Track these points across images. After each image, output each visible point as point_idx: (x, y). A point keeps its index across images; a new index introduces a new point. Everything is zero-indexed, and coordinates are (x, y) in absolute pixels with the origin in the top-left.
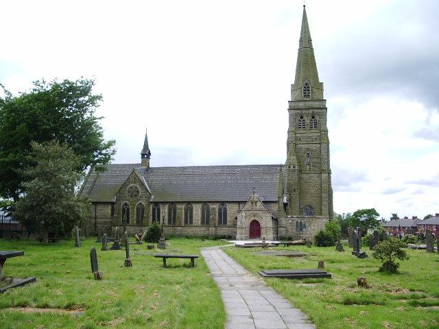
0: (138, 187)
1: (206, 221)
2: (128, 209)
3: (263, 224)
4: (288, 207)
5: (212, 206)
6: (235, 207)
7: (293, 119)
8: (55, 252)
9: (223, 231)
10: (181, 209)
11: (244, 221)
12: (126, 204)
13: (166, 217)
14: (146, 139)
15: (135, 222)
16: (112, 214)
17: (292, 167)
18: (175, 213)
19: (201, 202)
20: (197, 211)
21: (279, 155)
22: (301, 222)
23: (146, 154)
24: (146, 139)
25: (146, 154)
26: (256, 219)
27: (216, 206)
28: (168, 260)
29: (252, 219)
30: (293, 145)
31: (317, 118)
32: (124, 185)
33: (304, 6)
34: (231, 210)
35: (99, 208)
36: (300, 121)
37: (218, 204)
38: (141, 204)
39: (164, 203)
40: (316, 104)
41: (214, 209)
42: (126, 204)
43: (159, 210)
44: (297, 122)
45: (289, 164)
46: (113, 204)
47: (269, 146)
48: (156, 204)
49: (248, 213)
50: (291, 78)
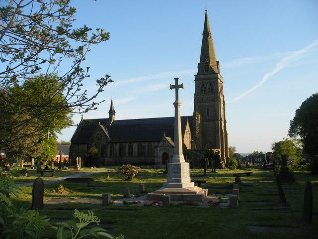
5: (124, 144)
13: (118, 151)
14: (206, 34)
15: (137, 154)
21: (175, 84)
23: (112, 112)
24: (206, 34)
25: (112, 112)
33: (206, 11)
37: (147, 143)
38: (103, 144)
39: (116, 143)
47: (108, 117)
49: (161, 148)
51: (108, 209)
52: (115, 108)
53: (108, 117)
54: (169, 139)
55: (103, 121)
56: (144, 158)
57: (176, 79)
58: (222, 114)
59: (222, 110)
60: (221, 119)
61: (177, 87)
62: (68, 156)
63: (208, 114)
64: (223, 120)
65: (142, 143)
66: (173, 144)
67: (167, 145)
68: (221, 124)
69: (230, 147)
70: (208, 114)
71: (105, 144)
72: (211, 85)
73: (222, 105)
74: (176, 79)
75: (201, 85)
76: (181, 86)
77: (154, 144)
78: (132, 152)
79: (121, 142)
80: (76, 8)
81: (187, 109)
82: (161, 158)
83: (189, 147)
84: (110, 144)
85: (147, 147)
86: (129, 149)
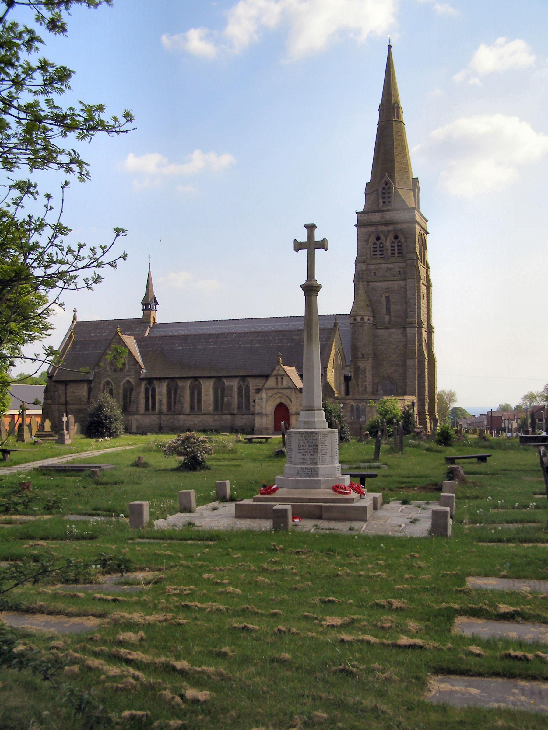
1: (219, 405)
4: (352, 383)
5: (227, 383)
7: (363, 241)
8: (32, 466)
9: (240, 421)
13: (165, 401)
16: (89, 399)
17: (358, 319)
19: (236, 377)
20: (208, 389)
21: (305, 240)
22: (358, 406)
23: (149, 303)
25: (149, 303)
26: (283, 401)
27: (234, 384)
29: (278, 401)
35: (71, 389)
36: (375, 244)
38: (128, 381)
39: (160, 379)
41: (231, 387)
43: (154, 390)
44: (371, 245)
45: (353, 315)
46: (89, 382)
47: (138, 314)
48: (150, 381)
49: (270, 393)
52: (157, 293)
53: (138, 314)
54: (291, 371)
55: (128, 325)
56: (229, 417)
57: (311, 228)
58: (424, 309)
59: (423, 302)
60: (420, 323)
61: (310, 245)
62: (40, 412)
63: (388, 310)
64: (425, 325)
65: (225, 380)
66: (299, 384)
67: (285, 384)
68: (420, 334)
69: (443, 392)
70: (388, 310)
71: (132, 381)
72: (396, 237)
73: (423, 288)
74: (311, 228)
75: (373, 239)
76: (323, 245)
77: (253, 384)
78: (199, 401)
79: (196, 378)
80: (55, 62)
81: (338, 298)
82: (271, 418)
83: (275, 507)
85: (235, 389)
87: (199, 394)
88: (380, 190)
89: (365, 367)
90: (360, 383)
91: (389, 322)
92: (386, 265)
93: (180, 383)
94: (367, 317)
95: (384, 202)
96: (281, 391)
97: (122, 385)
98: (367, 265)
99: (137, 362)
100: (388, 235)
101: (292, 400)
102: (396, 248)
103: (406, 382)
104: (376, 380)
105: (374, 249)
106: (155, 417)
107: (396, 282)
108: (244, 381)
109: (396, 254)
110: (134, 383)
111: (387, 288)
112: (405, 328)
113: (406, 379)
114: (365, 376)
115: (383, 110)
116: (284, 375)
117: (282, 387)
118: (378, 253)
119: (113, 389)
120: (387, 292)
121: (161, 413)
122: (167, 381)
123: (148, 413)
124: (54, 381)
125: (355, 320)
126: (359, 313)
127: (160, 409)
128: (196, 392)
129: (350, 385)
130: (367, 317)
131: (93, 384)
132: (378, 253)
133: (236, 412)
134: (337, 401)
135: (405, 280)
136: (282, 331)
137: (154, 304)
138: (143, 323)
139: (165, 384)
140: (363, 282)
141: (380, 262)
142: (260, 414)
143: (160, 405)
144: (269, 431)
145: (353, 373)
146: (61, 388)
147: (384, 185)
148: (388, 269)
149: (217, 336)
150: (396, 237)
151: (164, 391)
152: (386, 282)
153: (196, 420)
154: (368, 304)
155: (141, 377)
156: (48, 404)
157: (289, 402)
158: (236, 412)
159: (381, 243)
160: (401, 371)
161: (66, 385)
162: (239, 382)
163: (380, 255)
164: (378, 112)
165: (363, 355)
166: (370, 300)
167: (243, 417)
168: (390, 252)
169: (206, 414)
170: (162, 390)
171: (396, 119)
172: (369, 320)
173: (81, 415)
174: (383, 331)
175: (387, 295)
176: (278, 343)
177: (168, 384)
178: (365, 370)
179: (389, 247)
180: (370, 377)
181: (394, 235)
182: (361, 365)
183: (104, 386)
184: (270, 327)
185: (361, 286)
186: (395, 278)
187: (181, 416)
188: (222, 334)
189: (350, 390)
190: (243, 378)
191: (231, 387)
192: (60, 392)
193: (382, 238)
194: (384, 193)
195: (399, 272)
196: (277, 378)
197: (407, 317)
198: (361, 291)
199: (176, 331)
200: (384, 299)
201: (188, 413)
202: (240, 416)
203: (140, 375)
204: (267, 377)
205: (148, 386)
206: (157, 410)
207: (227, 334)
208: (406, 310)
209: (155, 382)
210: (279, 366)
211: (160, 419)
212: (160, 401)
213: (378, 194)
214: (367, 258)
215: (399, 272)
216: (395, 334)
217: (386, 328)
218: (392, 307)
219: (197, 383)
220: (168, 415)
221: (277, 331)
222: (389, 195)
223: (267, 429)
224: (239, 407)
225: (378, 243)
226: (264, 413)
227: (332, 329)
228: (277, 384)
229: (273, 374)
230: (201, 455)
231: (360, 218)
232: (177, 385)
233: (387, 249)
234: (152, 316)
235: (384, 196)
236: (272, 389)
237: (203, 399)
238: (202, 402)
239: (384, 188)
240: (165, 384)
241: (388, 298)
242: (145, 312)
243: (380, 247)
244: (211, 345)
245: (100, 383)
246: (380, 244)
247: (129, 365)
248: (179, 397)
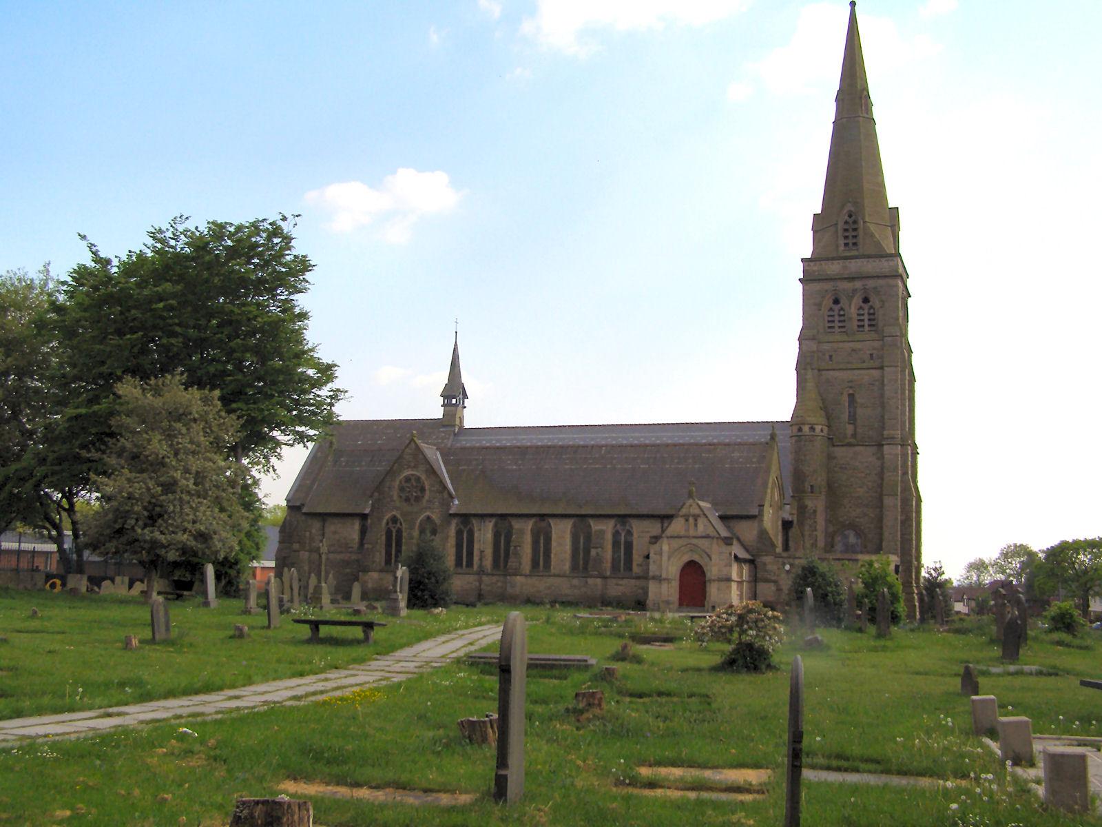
0: (423, 477)
1: (582, 562)
2: (399, 532)
3: (712, 571)
4: (794, 531)
5: (596, 526)
6: (654, 528)
9: (620, 587)
10: (524, 532)
11: (668, 564)
12: (394, 520)
13: (489, 552)
14: (456, 345)
16: (361, 543)
17: (806, 429)
18: (508, 542)
20: (562, 535)
23: (454, 392)
24: (456, 345)
25: (454, 392)
26: (696, 558)
27: (608, 527)
28: (324, 630)
29: (686, 558)
30: (811, 365)
31: (875, 301)
32: (391, 473)
34: (641, 532)
35: (332, 527)
36: (831, 309)
37: (612, 523)
38: (428, 518)
40: (869, 266)
41: (602, 532)
42: (394, 520)
45: (798, 420)
46: (364, 517)
47: (745, 373)
48: (465, 518)
49: (676, 543)
50: (811, 197)
51: (291, 580)
53: (438, 413)
56: (599, 581)
63: (853, 418)
65: (592, 522)
70: (853, 418)
71: (434, 517)
72: (866, 300)
75: (828, 302)
79: (542, 517)
82: (675, 584)
84: (454, 522)
85: (609, 537)
86: (535, 543)
87: (548, 540)
88: (841, 225)
89: (816, 507)
90: (807, 533)
91: (854, 435)
92: (852, 345)
93: (517, 525)
94: (820, 427)
95: (846, 245)
96: (695, 541)
97: (418, 524)
98: (819, 342)
99: (445, 487)
100: (852, 297)
101: (713, 557)
102: (866, 317)
103: (881, 534)
104: (831, 529)
105: (830, 319)
106: (471, 578)
107: (868, 371)
108: (624, 524)
109: (867, 328)
110: (438, 522)
111: (851, 381)
112: (880, 445)
113: (881, 528)
114: (816, 522)
115: (843, 100)
116: (699, 516)
117: (695, 534)
118: (837, 324)
119: (404, 530)
120: (851, 387)
121: (481, 572)
122: (494, 520)
123: (459, 570)
124: (305, 514)
125: (800, 430)
126: (808, 419)
127: (481, 566)
128: (542, 538)
129: (790, 534)
130: (820, 427)
131: (369, 521)
132: (837, 324)
133: (608, 574)
134: (781, 560)
135: (882, 368)
136: (683, 445)
137: (461, 396)
138: (444, 426)
139: (490, 526)
140: (812, 369)
141: (839, 338)
142: (659, 579)
143: (481, 559)
144: (671, 606)
145: (795, 516)
146: (316, 525)
147: (846, 217)
148: (853, 350)
149: (576, 449)
150: (866, 300)
151: (489, 536)
152: (845, 372)
153: (539, 585)
154: (821, 405)
155: (451, 512)
156: (295, 551)
157: (707, 559)
158: (608, 574)
159: (842, 309)
160: (873, 516)
161: (324, 521)
162: (616, 525)
163: (840, 327)
164: (834, 105)
165: (812, 486)
166: (823, 400)
167: (620, 582)
168: (856, 323)
169: (559, 576)
170: (484, 535)
171: (865, 115)
172: (822, 431)
173: (348, 570)
174: (844, 449)
175: (851, 392)
176: (678, 463)
177: (496, 525)
178: (815, 511)
179: (855, 316)
180: (823, 523)
181: (863, 296)
182: (809, 503)
183: (387, 524)
184: (666, 438)
185: (810, 374)
186: (865, 365)
187: (518, 577)
188: (583, 447)
189: (791, 544)
190: (623, 518)
191: (602, 532)
192: (314, 531)
193: (844, 302)
194: (855, 230)
195: (871, 355)
196: (687, 520)
197: (883, 428)
198: (810, 385)
199: (498, 441)
200: (845, 398)
201: (528, 572)
202: (614, 581)
203: (449, 509)
204: (669, 517)
205: (462, 527)
206: (475, 567)
207: (593, 447)
208: (883, 417)
209: (474, 521)
210: (691, 501)
211: (480, 582)
212: (482, 552)
213: (836, 232)
214: (818, 331)
215: (871, 355)
216: (865, 456)
217: (850, 445)
218: (859, 411)
219: (544, 524)
220: (493, 575)
221: (675, 445)
222: (854, 234)
223: (668, 603)
224: (615, 567)
225: (836, 308)
226: (664, 576)
227: (767, 443)
228: (687, 530)
229: (681, 513)
230: (772, 644)
231: (807, 268)
232: (511, 526)
233: (850, 319)
234: (458, 416)
235: (847, 234)
236: (679, 537)
237: (553, 551)
238: (552, 556)
239: (846, 222)
240: (490, 526)
241: (851, 396)
242: (447, 408)
243: (869, 314)
244: (566, 464)
245: (380, 519)
246: (840, 310)
247: (431, 491)
248: (515, 547)
